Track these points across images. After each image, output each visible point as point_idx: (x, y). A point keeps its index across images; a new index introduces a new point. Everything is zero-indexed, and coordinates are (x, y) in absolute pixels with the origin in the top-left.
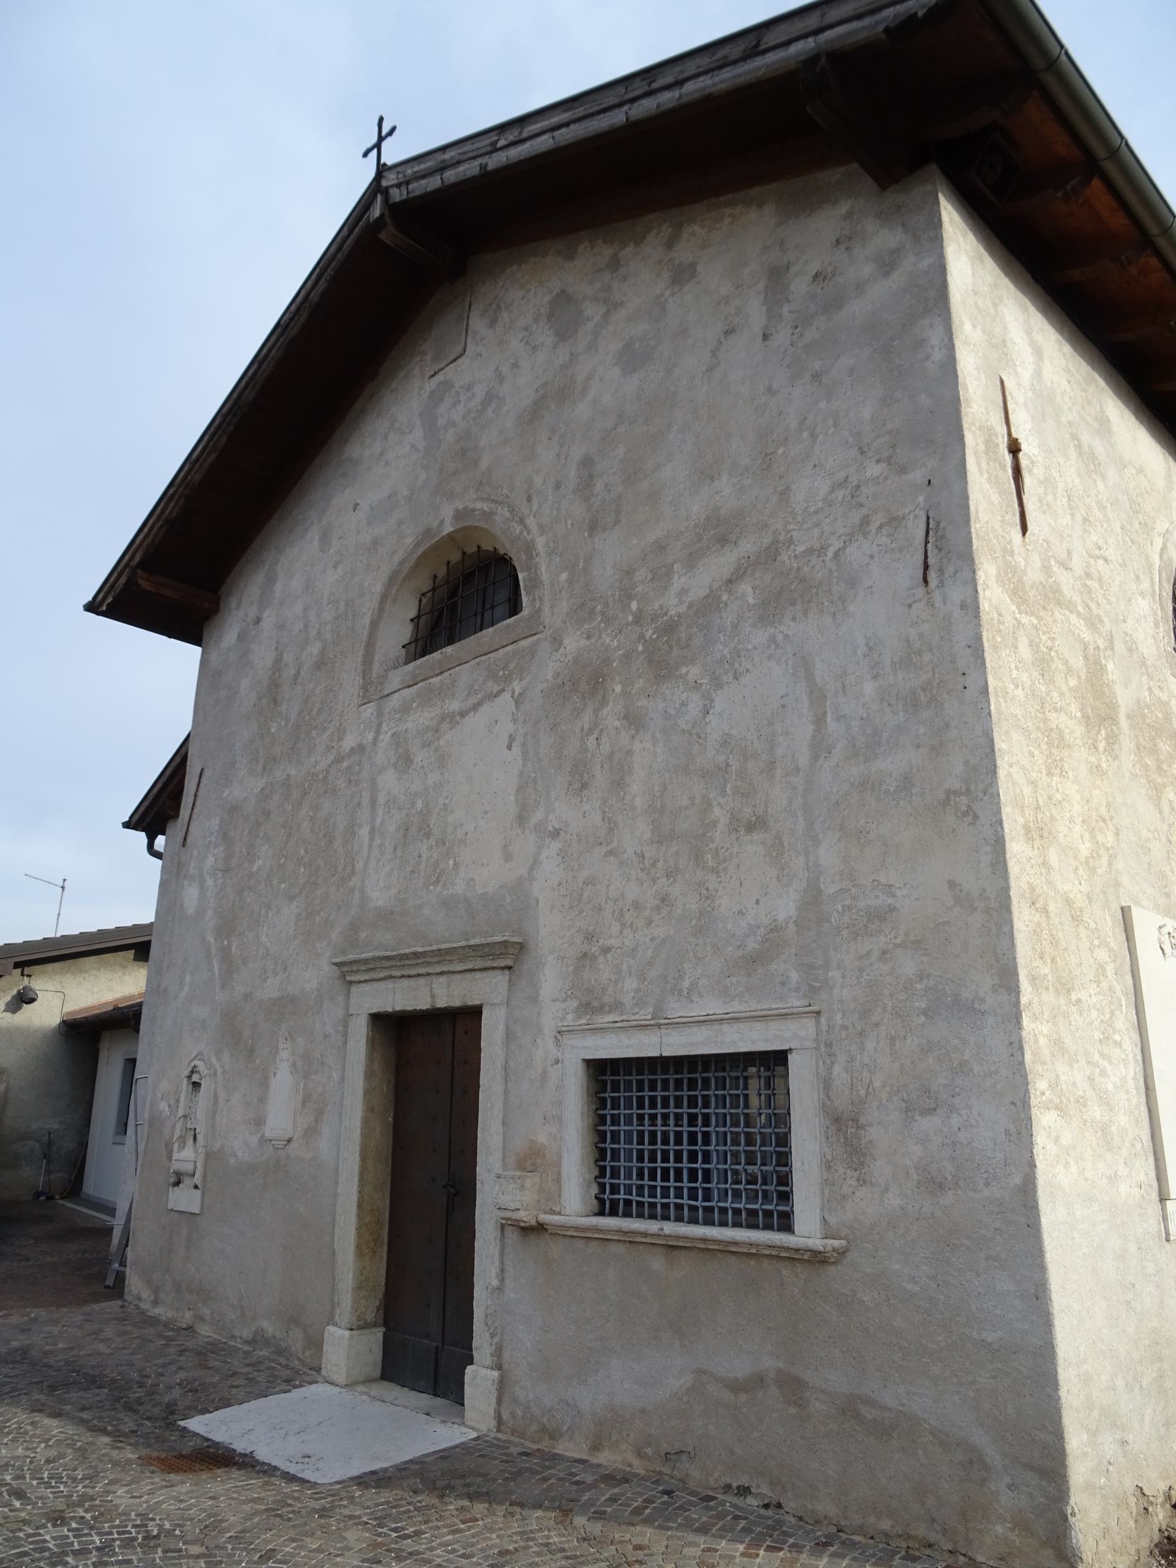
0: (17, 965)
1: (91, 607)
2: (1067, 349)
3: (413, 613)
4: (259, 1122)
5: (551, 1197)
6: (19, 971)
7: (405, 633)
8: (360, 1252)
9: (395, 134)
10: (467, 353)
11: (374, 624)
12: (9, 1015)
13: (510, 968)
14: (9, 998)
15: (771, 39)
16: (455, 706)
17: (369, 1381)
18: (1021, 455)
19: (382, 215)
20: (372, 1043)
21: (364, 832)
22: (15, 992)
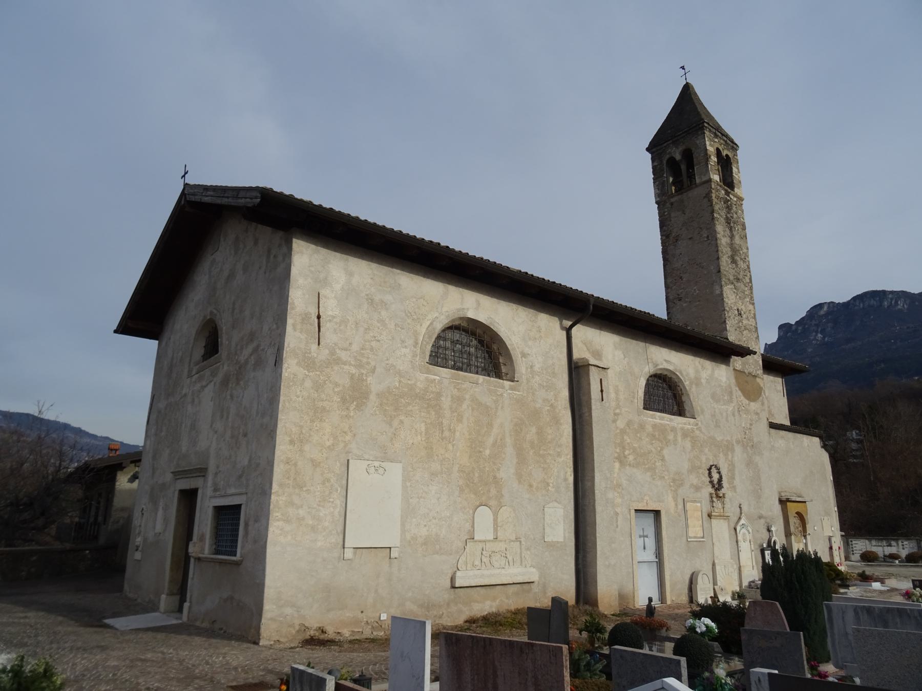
0: (132, 462)
1: (116, 332)
2: (374, 266)
3: (204, 345)
4: (154, 528)
5: (202, 551)
6: (133, 464)
7: (202, 351)
8: (172, 569)
9: (188, 173)
10: (219, 250)
11: (192, 348)
12: (130, 484)
13: (204, 476)
14: (129, 476)
15: (242, 194)
16: (204, 383)
17: (173, 612)
18: (321, 319)
19: (184, 204)
20: (179, 500)
21: (183, 425)
22: (132, 474)
